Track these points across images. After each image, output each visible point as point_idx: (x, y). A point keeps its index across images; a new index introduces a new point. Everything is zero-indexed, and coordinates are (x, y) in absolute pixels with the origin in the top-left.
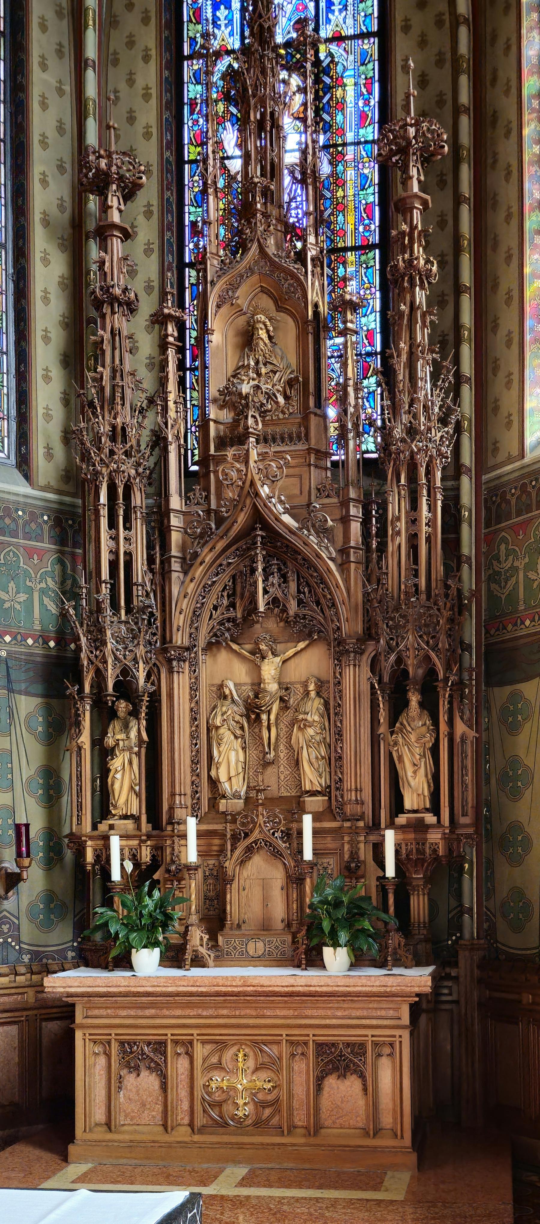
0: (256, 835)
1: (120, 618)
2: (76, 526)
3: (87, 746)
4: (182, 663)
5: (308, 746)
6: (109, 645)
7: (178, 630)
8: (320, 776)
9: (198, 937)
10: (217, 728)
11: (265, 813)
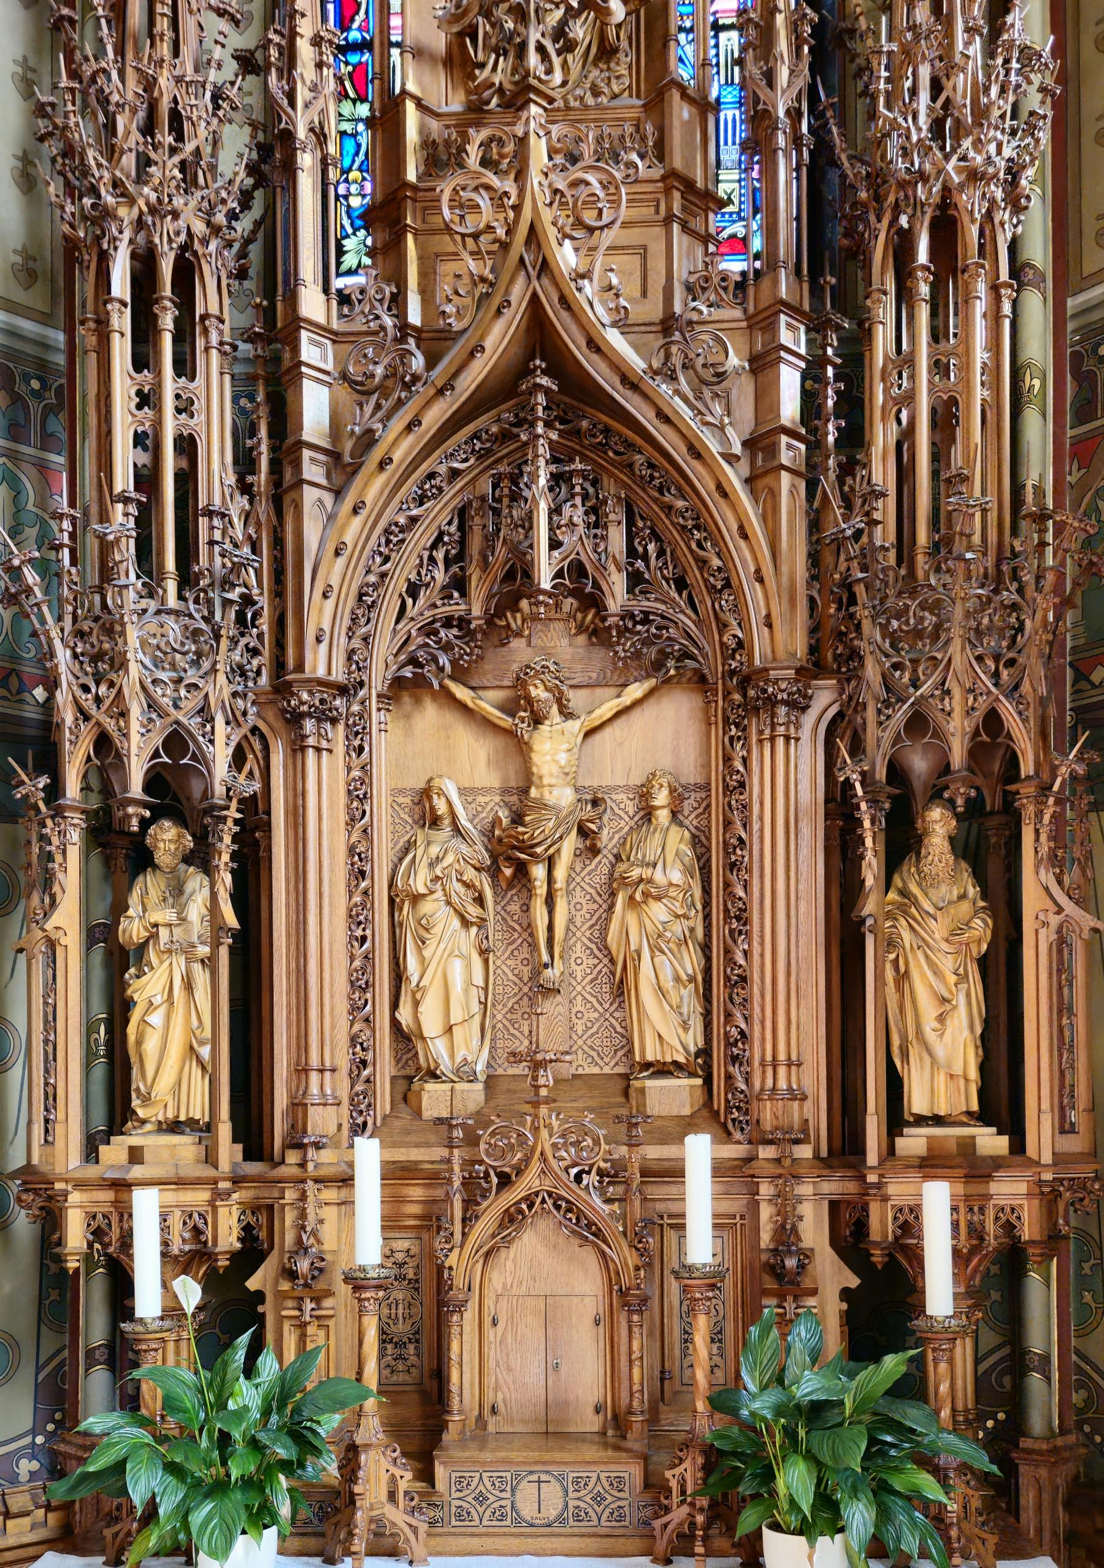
0: (530, 1181)
1: (163, 602)
2: (51, 398)
3: (72, 940)
4: (328, 726)
5: (655, 949)
6: (133, 668)
7: (319, 640)
8: (685, 1026)
9: (385, 1478)
10: (416, 899)
11: (555, 1123)
